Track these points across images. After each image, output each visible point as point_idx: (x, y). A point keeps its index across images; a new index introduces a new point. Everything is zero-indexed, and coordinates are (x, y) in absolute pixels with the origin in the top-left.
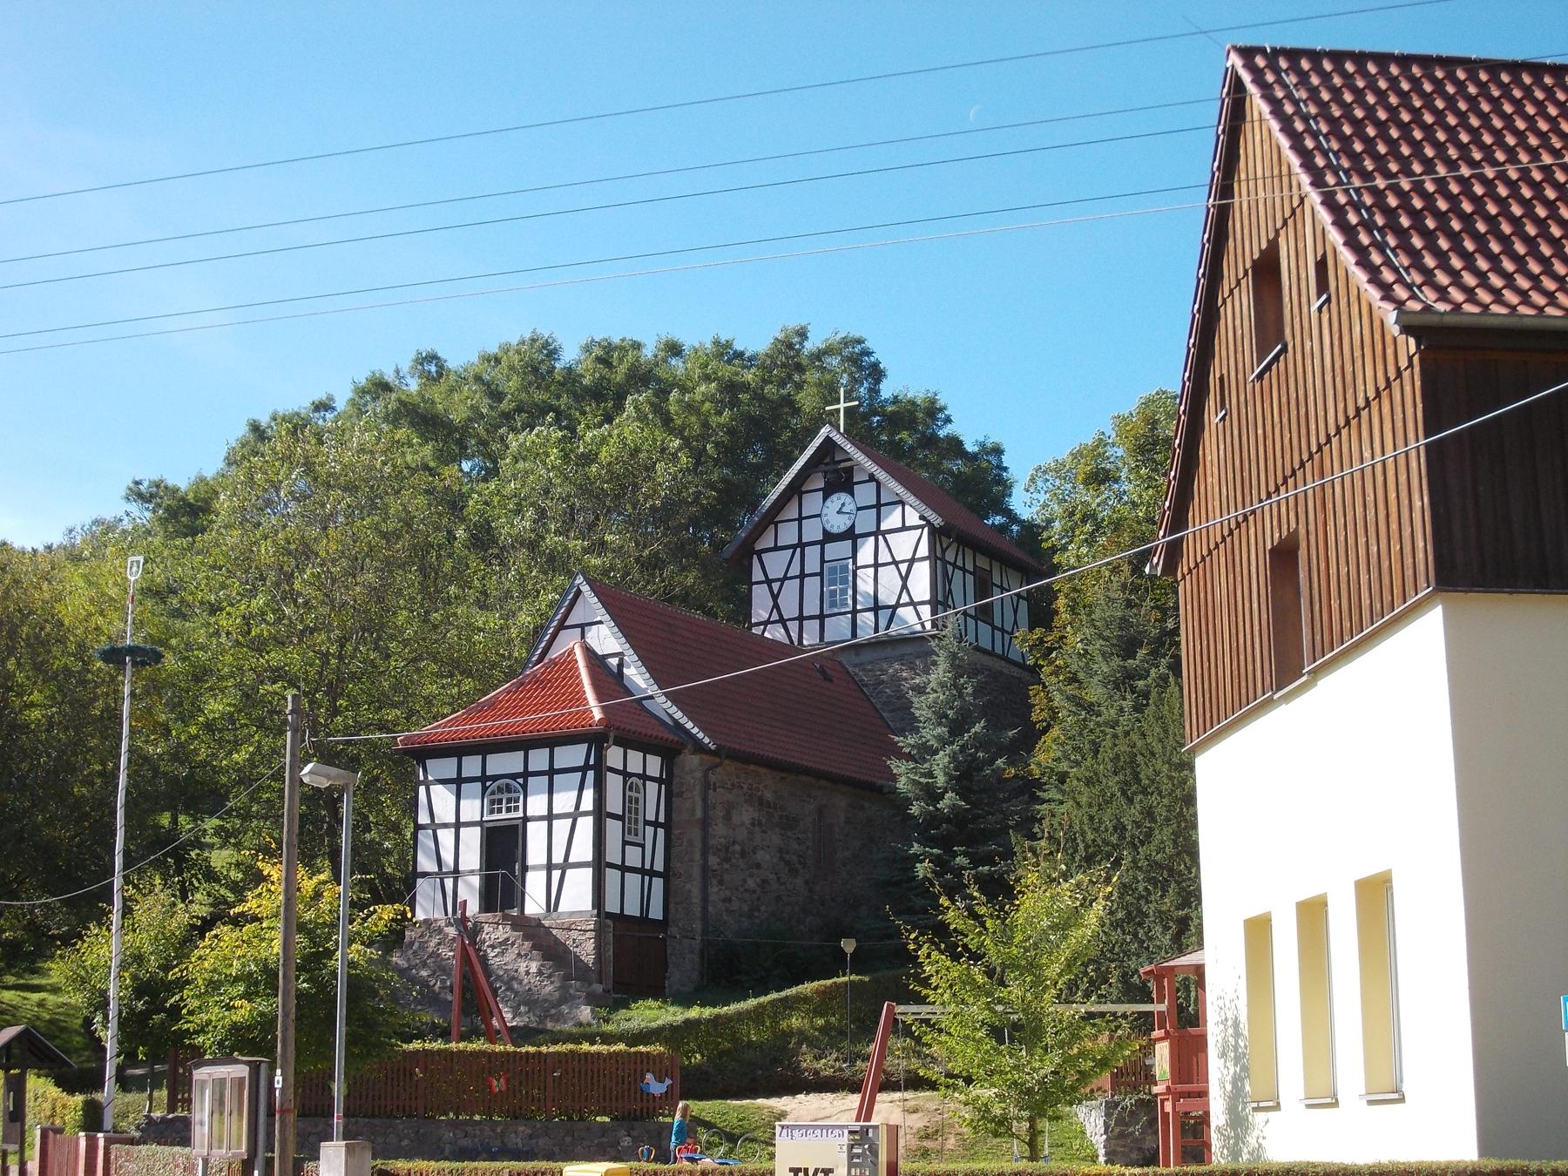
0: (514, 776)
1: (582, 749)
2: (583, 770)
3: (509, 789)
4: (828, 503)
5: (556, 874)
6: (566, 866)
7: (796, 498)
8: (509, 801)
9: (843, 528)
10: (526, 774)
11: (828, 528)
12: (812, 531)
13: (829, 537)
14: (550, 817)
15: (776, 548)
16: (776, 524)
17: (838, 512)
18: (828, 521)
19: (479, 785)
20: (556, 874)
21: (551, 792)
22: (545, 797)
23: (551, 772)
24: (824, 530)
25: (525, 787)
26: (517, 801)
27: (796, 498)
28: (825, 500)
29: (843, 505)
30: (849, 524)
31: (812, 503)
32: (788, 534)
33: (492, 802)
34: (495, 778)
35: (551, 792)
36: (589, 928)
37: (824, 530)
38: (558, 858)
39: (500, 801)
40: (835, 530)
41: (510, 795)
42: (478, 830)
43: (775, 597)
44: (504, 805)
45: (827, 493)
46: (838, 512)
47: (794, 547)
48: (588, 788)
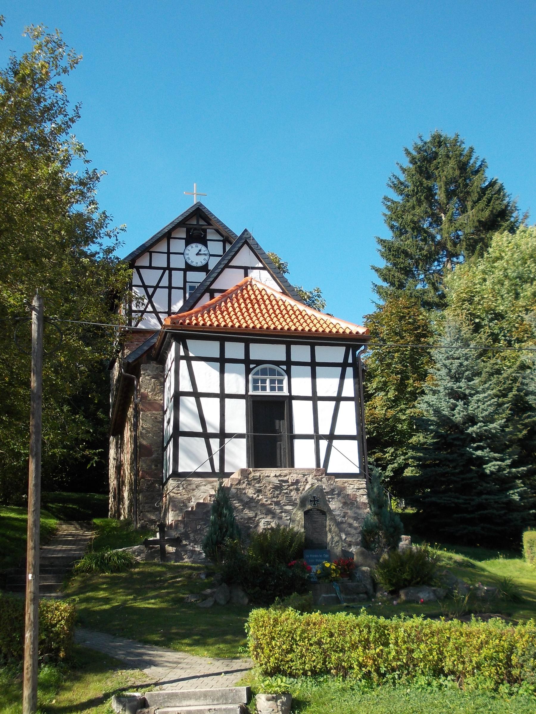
0: (278, 363)
1: (342, 350)
2: (344, 365)
3: (272, 372)
4: (189, 247)
5: (324, 444)
6: (331, 437)
7: (222, 239)
8: (272, 382)
9: (200, 264)
10: (289, 363)
11: (189, 262)
12: (177, 262)
13: (189, 268)
14: (315, 398)
15: (150, 267)
16: (151, 253)
17: (197, 254)
18: (189, 258)
19: (243, 366)
20: (324, 444)
21: (314, 376)
22: (337, 381)
23: (313, 364)
24: (186, 263)
25: (288, 373)
26: (281, 382)
27: (222, 239)
28: (187, 245)
29: (200, 250)
30: (204, 262)
31: (178, 245)
32: (160, 260)
33: (255, 381)
34: (259, 363)
35: (314, 376)
36: (361, 486)
37: (186, 263)
38: (324, 430)
39: (264, 381)
40: (194, 264)
41: (273, 377)
42: (243, 402)
43: (150, 297)
44: (277, 385)
45: (189, 242)
46: (197, 254)
47: (164, 269)
48: (349, 378)
